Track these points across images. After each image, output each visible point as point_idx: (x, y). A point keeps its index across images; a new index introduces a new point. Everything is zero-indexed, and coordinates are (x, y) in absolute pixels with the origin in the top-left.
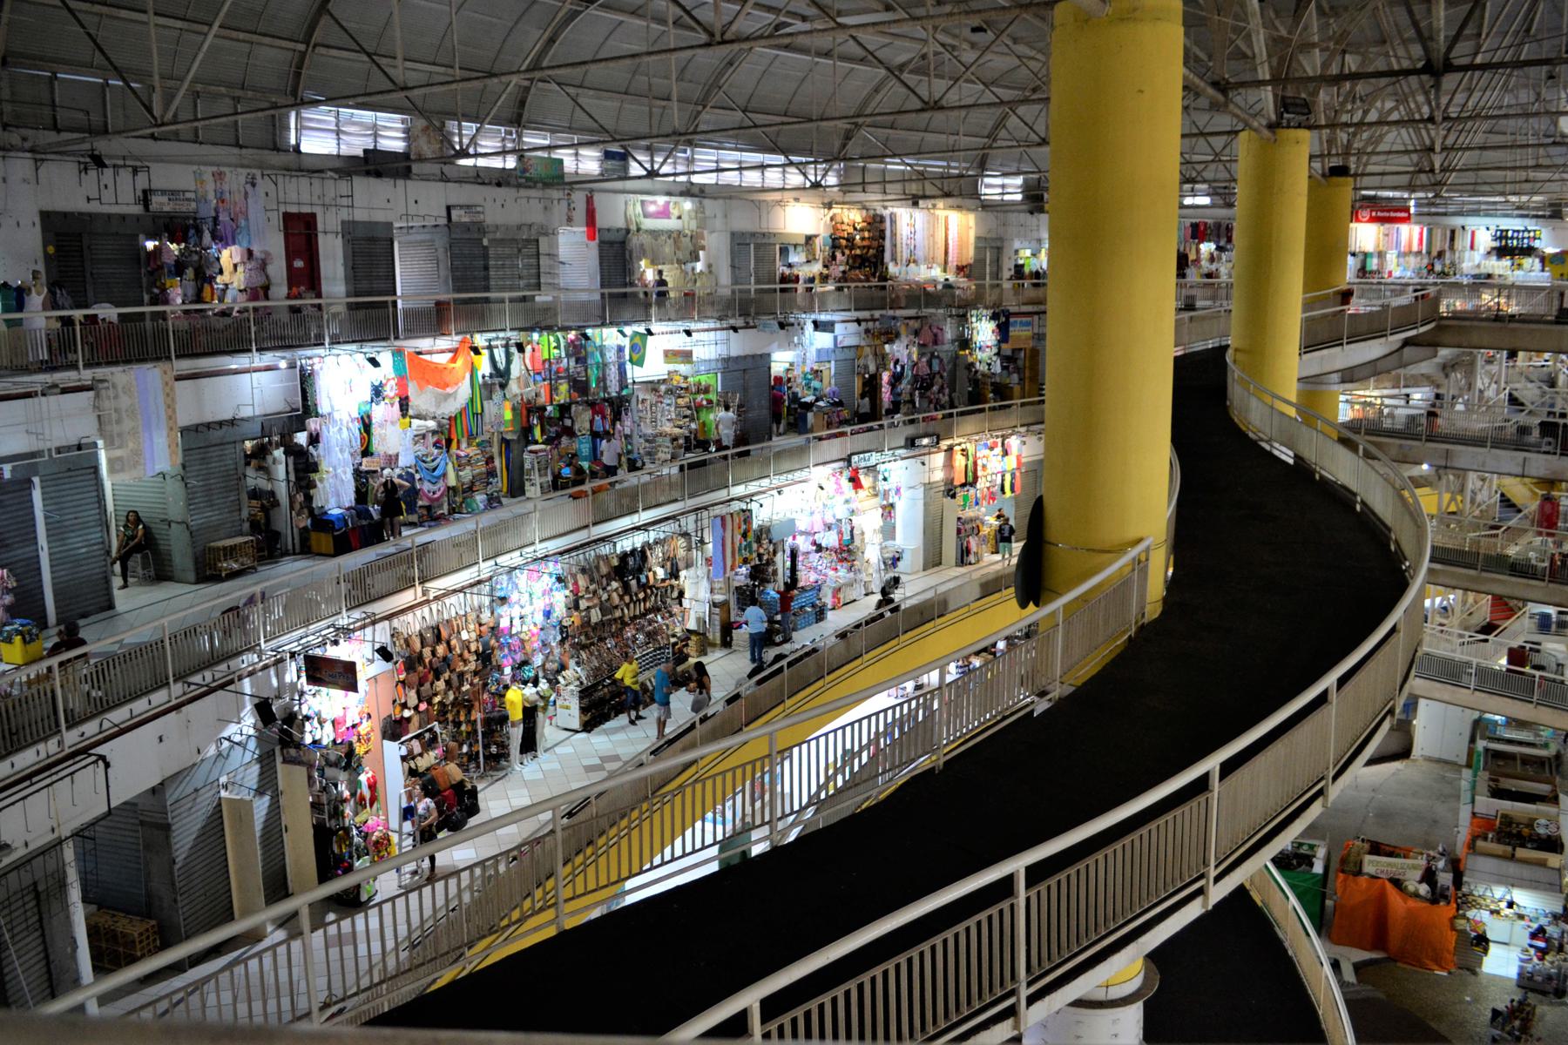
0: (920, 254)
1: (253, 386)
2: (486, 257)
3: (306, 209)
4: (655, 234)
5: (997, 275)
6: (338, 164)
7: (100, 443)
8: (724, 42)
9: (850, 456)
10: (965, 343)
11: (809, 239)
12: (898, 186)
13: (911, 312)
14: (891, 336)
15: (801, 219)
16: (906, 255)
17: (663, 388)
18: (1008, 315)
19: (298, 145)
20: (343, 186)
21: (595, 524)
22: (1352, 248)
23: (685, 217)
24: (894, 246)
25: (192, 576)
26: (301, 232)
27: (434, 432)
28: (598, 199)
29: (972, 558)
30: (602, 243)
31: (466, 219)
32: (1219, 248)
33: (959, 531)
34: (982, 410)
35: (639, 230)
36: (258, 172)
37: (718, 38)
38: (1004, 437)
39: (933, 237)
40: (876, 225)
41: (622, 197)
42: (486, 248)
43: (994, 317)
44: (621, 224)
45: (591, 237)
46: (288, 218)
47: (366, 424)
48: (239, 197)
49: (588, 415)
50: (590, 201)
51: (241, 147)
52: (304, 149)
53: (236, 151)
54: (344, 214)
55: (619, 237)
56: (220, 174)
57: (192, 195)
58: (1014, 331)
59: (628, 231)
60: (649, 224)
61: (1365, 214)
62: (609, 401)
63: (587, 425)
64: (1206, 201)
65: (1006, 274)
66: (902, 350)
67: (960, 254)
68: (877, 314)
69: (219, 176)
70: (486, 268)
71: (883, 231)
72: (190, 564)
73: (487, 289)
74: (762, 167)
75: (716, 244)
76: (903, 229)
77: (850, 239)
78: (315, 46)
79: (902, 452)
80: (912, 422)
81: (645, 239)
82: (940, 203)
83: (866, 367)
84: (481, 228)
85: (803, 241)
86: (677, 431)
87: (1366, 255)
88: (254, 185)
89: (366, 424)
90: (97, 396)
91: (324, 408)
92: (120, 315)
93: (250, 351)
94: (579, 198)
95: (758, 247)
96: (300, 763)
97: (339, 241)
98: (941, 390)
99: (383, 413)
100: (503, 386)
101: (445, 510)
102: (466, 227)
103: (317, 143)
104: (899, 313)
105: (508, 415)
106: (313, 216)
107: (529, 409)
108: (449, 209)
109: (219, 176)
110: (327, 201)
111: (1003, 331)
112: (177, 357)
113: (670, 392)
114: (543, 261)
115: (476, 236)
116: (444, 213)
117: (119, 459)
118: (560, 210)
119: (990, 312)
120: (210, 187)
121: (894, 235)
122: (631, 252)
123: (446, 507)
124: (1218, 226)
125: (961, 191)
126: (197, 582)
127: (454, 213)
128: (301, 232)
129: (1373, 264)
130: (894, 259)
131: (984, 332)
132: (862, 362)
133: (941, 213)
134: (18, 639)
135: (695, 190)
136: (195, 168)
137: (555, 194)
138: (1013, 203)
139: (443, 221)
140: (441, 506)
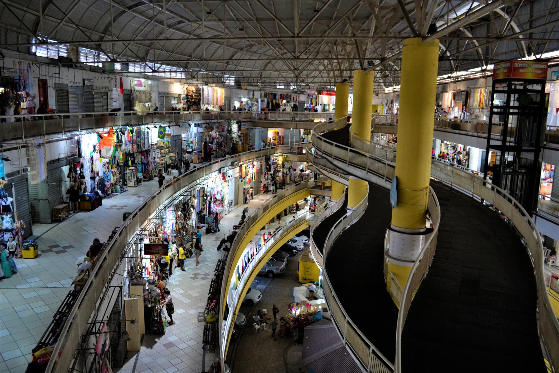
0: (210, 101)
1: (62, 147)
2: (93, 98)
3: (44, 78)
4: (140, 92)
5: (229, 109)
6: (48, 61)
7: (29, 168)
8: (298, 37)
9: (220, 169)
10: (230, 132)
11: (179, 95)
12: (201, 79)
13: (215, 121)
14: (212, 129)
15: (178, 89)
16: (206, 102)
17: (155, 146)
18: (240, 122)
19: (35, 52)
20: (56, 70)
21: (174, 194)
22: (320, 103)
23: (146, 86)
24: (203, 98)
25: (50, 221)
26: (43, 85)
27: (108, 163)
28: (124, 79)
29: (248, 201)
30: (124, 94)
31: (89, 84)
32: (288, 102)
33: (244, 193)
34: (347, 149)
35: (134, 90)
36: (31, 62)
37: (296, 35)
38: (253, 162)
39: (214, 95)
40: (199, 92)
41: (129, 78)
42: (93, 95)
43: (237, 123)
44: (129, 88)
45: (122, 93)
46: (39, 80)
47: (92, 158)
48: (25, 72)
49: (140, 156)
50: (121, 79)
51: (20, 52)
52: (38, 54)
53: (18, 53)
54: (57, 81)
55: (129, 93)
56: (21, 62)
57: (13, 70)
58: (242, 128)
59: (131, 90)
60: (138, 88)
61: (324, 93)
62: (145, 151)
63: (140, 160)
64: (283, 87)
65: (232, 109)
66: (214, 134)
67: (221, 103)
68: (208, 121)
69: (20, 63)
70: (93, 103)
71: (200, 93)
72: (49, 216)
73: (94, 111)
74: (176, 72)
75: (155, 96)
76: (206, 93)
77: (192, 96)
78: (45, 15)
79: (230, 167)
80: (232, 157)
81: (137, 93)
82: (214, 85)
83: (206, 139)
84: (91, 87)
85: (178, 96)
86: (162, 161)
87: (325, 105)
88: (30, 67)
89: (92, 158)
90: (28, 150)
91: (83, 154)
92: (32, 117)
93: (62, 132)
94: (118, 77)
95: (166, 97)
96: (139, 285)
97: (54, 91)
98: (224, 147)
99: (96, 155)
100: (120, 146)
101: (110, 192)
102: (89, 87)
103: (41, 52)
104: (213, 121)
105: (121, 157)
106: (46, 80)
107: (127, 155)
108: (84, 80)
109: (20, 63)
110: (50, 75)
111: (239, 127)
112: (46, 134)
113: (158, 148)
114: (109, 100)
115: (91, 90)
116: (82, 82)
117: (35, 175)
118: (113, 82)
119: (235, 121)
120: (18, 67)
121: (203, 95)
122: (133, 99)
123: (110, 190)
124: (287, 95)
125: (220, 82)
126: (53, 222)
127: (86, 82)
128: (43, 85)
129: (327, 108)
130: (203, 103)
131: (235, 127)
132: (204, 137)
133: (216, 88)
134: (32, 248)
135: (146, 77)
136: (13, 59)
137: (112, 76)
138: (232, 86)
139: (82, 85)
140: (109, 191)
